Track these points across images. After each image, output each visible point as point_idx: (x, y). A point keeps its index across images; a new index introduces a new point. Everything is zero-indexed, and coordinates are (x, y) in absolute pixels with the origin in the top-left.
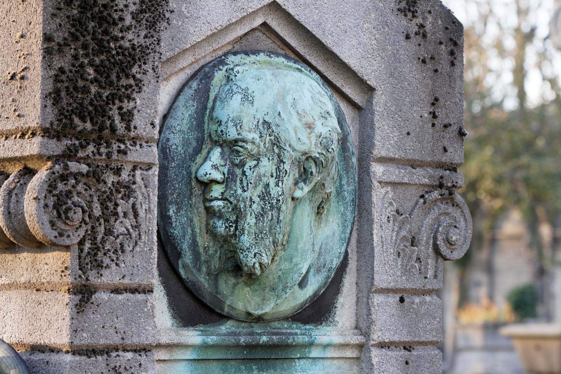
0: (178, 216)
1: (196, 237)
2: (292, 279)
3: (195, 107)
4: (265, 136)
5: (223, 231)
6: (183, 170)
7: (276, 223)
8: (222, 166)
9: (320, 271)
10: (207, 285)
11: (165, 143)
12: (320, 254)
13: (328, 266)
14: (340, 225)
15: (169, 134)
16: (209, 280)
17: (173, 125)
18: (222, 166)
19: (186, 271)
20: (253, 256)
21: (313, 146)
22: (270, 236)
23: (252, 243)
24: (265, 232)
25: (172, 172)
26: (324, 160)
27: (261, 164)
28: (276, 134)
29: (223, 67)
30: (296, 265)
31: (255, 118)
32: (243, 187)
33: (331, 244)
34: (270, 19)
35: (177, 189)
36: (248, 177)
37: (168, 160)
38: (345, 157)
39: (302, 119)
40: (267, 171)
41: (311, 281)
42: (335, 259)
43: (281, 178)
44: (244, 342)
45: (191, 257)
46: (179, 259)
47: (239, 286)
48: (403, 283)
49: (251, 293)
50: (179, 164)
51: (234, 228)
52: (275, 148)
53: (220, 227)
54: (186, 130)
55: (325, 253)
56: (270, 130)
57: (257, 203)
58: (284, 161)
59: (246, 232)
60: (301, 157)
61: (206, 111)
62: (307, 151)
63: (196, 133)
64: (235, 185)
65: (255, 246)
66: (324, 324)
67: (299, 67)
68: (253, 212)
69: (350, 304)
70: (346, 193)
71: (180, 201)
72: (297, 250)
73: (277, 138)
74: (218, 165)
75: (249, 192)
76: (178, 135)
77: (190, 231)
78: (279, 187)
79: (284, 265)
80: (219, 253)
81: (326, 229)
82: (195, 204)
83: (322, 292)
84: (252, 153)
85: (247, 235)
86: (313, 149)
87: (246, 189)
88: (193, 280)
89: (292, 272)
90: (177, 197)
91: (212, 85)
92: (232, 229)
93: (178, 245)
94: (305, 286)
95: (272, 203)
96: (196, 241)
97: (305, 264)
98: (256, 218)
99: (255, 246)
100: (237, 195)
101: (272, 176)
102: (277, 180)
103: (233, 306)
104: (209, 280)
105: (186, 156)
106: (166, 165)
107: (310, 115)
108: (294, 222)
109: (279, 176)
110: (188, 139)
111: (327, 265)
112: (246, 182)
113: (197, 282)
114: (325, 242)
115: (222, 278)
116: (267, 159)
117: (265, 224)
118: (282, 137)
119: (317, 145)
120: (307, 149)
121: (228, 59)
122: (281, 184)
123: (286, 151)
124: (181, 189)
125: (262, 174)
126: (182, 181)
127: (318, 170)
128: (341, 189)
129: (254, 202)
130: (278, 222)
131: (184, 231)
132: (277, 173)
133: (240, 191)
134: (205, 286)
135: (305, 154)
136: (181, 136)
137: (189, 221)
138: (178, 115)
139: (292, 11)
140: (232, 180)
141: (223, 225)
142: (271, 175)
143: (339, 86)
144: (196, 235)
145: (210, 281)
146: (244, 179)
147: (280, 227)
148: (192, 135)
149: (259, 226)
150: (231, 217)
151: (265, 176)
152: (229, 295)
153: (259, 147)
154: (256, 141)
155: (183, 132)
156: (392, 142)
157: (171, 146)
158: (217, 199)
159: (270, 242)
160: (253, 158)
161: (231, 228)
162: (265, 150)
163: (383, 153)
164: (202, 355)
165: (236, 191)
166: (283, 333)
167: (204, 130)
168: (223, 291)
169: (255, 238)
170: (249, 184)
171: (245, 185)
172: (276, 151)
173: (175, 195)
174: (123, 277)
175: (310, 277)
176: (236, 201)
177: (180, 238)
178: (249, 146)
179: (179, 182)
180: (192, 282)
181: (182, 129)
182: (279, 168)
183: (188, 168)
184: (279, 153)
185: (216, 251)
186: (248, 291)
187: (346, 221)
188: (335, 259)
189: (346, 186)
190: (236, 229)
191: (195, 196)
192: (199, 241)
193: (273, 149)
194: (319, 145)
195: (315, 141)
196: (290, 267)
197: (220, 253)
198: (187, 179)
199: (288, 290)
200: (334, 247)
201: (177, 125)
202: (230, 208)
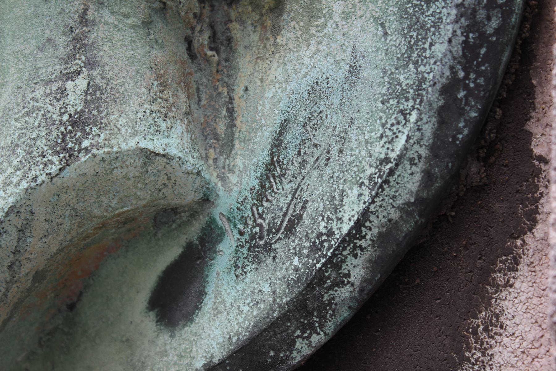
9: (268, 248)
14: (393, 25)
41: (218, 294)
42: (356, 191)
81: (306, 52)
94: (189, 318)
114: (306, 114)
175: (212, 278)
188: (356, 191)
200: (353, 134)
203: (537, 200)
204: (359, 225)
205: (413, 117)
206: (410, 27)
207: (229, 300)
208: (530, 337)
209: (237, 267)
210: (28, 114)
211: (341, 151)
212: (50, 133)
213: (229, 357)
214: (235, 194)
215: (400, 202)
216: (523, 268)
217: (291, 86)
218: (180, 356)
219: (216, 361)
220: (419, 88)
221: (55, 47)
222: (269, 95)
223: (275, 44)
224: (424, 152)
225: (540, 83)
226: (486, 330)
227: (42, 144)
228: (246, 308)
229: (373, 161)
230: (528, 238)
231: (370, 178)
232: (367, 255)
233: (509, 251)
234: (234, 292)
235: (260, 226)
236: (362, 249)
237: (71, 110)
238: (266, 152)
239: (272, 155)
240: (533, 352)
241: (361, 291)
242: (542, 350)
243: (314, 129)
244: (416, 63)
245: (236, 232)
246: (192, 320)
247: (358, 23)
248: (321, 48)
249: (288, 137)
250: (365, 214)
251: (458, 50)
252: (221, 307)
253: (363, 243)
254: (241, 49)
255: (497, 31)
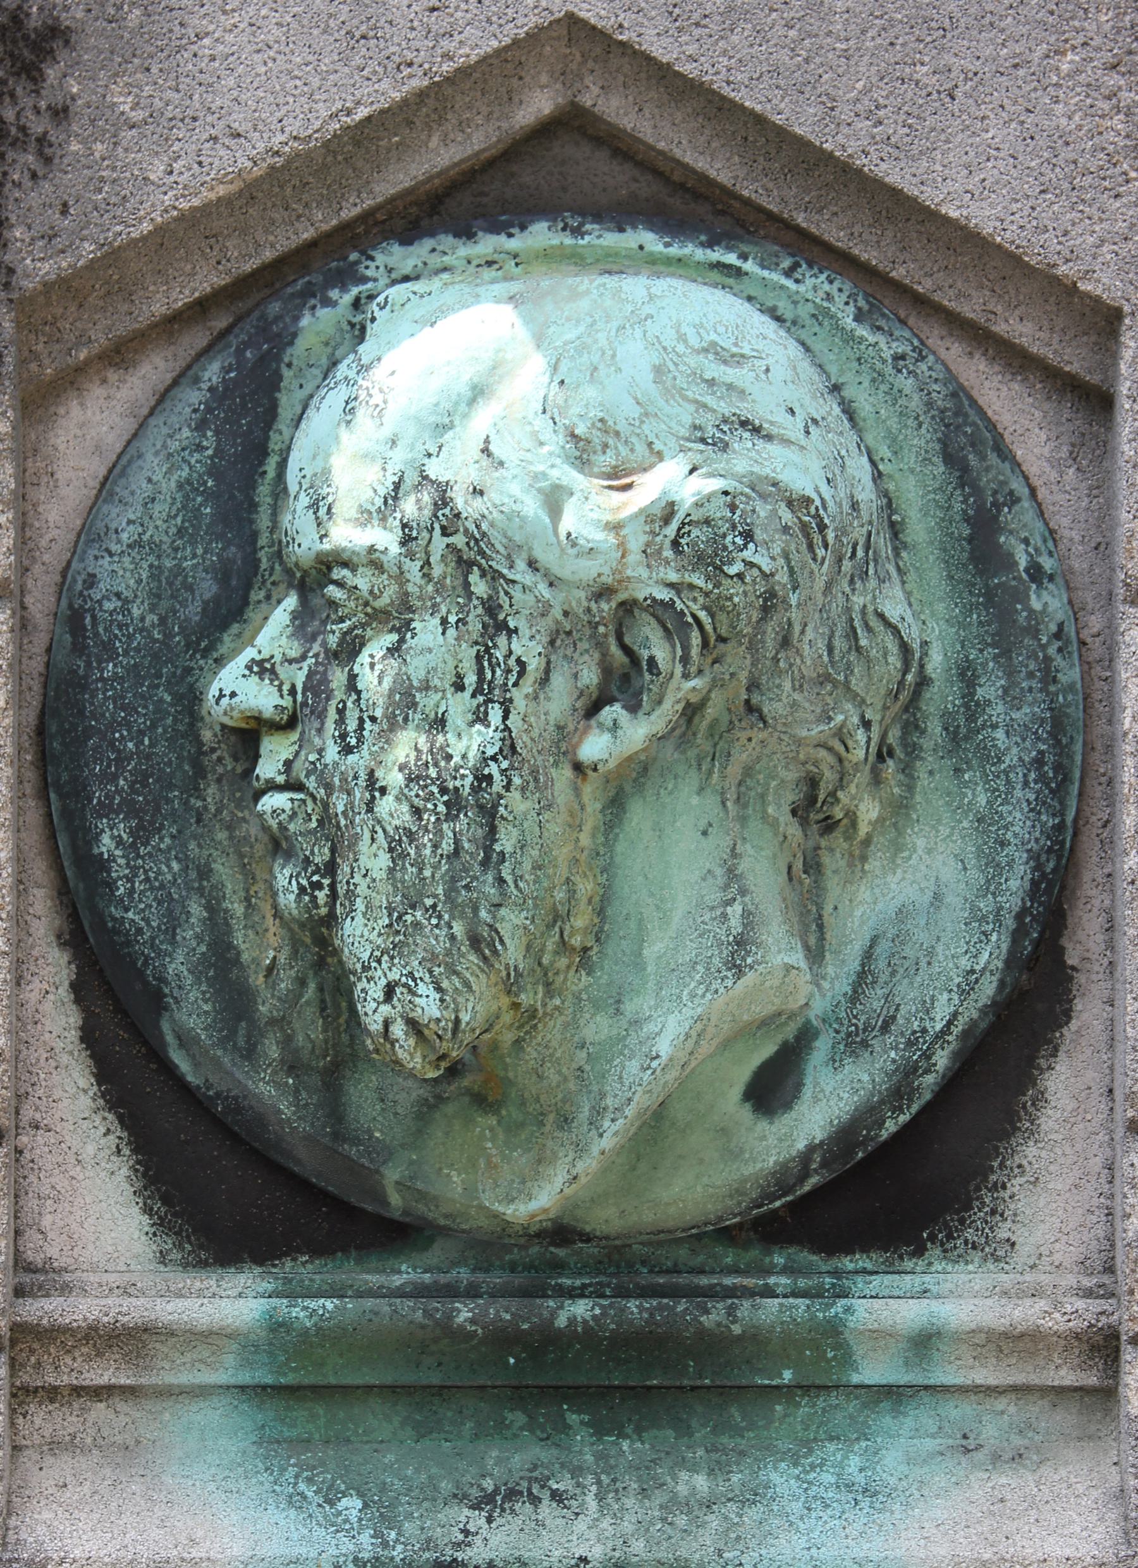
0: (138, 856)
1: (229, 930)
2: (621, 1078)
3: (210, 452)
4: (425, 534)
5: (293, 905)
6: (157, 686)
7: (477, 867)
8: (291, 662)
9: (865, 1044)
10: (286, 1109)
11: (81, 594)
12: (863, 978)
13: (908, 1020)
14: (972, 862)
15: (96, 558)
16: (297, 1092)
17: (113, 526)
18: (291, 662)
19: (193, 1057)
20: (380, 995)
21: (634, 557)
22: (453, 917)
23: (378, 947)
24: (429, 902)
25: (106, 698)
26: (704, 608)
27: (410, 642)
28: (472, 527)
29: (344, 289)
30: (636, 1023)
31: (384, 469)
32: (343, 736)
33: (922, 937)
34: (595, 90)
35: (129, 759)
36: (364, 695)
37: (89, 656)
38: (989, 595)
39: (593, 458)
40: (435, 669)
41: (816, 1084)
42: (945, 996)
43: (497, 692)
44: (472, 1321)
45: (206, 1008)
46: (159, 1015)
47: (450, 1109)
49: (501, 1136)
50: (136, 665)
51: (326, 891)
52: (474, 577)
53: (286, 890)
54: (165, 539)
55: (893, 973)
56: (447, 511)
57: (394, 792)
58: (512, 625)
59: (360, 905)
60: (593, 605)
61: (261, 463)
62: (608, 580)
63: (217, 546)
64: (320, 731)
65: (392, 958)
66: (933, 1252)
67: (731, 258)
68: (378, 828)
69: (1078, 1174)
70: (1000, 734)
71: (147, 802)
72: (639, 965)
73: (476, 541)
74: (278, 659)
75: (365, 753)
76: (126, 560)
77: (196, 909)
78: (488, 726)
79: (592, 1025)
80: (312, 986)
81: (893, 880)
82: (219, 811)
83: (891, 1127)
84: (379, 603)
85: (364, 914)
86: (636, 568)
87: (353, 742)
88: (229, 1090)
89: (622, 1053)
90: (131, 787)
91: (289, 365)
92: (322, 896)
93: (146, 963)
94: (788, 1106)
95: (456, 789)
96: (230, 946)
97: (672, 1020)
98: (391, 850)
99: (392, 958)
100: (326, 765)
101: (459, 687)
102: (481, 699)
103: (419, 1185)
104: (297, 1092)
105: (168, 635)
106: (81, 672)
107: (634, 439)
108: (618, 859)
109: (490, 682)
110: (178, 570)
111: (901, 1021)
112: (357, 714)
113: (245, 1097)
114: (895, 931)
115: (359, 1081)
116: (436, 621)
117: (427, 873)
118: (493, 533)
119: (659, 552)
120: (606, 570)
121: (372, 259)
122: (500, 713)
123: (518, 587)
124: (148, 757)
125: (415, 683)
126: (154, 726)
127: (679, 653)
128: (971, 718)
129: (383, 791)
130: (485, 863)
131: (170, 912)
132: (480, 672)
133: (332, 753)
134: (280, 1112)
135: (603, 592)
136: (145, 565)
137: (193, 875)
138: (134, 487)
139: (660, 49)
140: (312, 712)
141: (294, 882)
142: (454, 685)
143: (972, 315)
144: (227, 924)
145: (304, 1095)
146: (349, 704)
147: (501, 881)
148: (194, 556)
149: (403, 882)
150: (316, 850)
151: (427, 688)
152: (402, 1146)
153: (400, 577)
154: (383, 558)
155: (155, 547)
157: (99, 602)
158: (272, 786)
159: (453, 938)
160: (387, 622)
161: (317, 893)
162: (430, 588)
164: (295, 1370)
165: (320, 751)
166: (698, 1287)
167: (255, 535)
168: (369, 1132)
169: (390, 925)
170: (368, 725)
171: (352, 725)
172: (480, 587)
173: (122, 782)
175: (809, 1069)
176: (322, 791)
177: (153, 938)
178: (362, 581)
179: (141, 733)
180: (227, 1098)
181: (145, 538)
182: (490, 655)
183: (182, 678)
184: (490, 598)
185: (302, 982)
186: (492, 1130)
187: (1003, 844)
188: (945, 996)
189: (1000, 708)
190: (333, 895)
191: (219, 781)
192: (243, 947)
193: (467, 585)
194: (668, 553)
195: (644, 538)
196: (615, 1032)
197: (321, 989)
198: (175, 720)
199: (607, 1124)
200: (940, 949)
201: (124, 524)
202: (314, 818)
203: (1071, 1001)
204: (950, 1023)
205: (994, 937)
206: (987, 865)
207: (828, 1089)
208: (1069, 1108)
209: (834, 1061)
210: (700, 936)
211: (929, 963)
212: (721, 952)
213: (830, 1138)
214: (828, 998)
215: (980, 1004)
216: (1061, 1055)
217: (880, 906)
218: (780, 1140)
219: (817, 1141)
220: (998, 914)
221: (714, 877)
222: (858, 913)
223: (863, 870)
224: (1000, 965)
225: (1070, 908)
226: (1033, 1104)
227: (716, 961)
228: (846, 1095)
229: (960, 971)
230: (1065, 1030)
231: (959, 986)
232: (952, 1047)
233: (1049, 1042)
234: (832, 1082)
235: (856, 1025)
236: (949, 1043)
237: (734, 932)
238: (857, 962)
239: (863, 965)
240: (1072, 1120)
241: (944, 1076)
242: (1080, 1118)
243: (902, 943)
244: (994, 894)
245: (831, 1031)
246: (791, 1108)
247: (940, 858)
248: (907, 876)
249: (878, 950)
250: (955, 1015)
251: (1027, 885)
252: (821, 1096)
253: (950, 1038)
254: (829, 873)
255: (1054, 871)
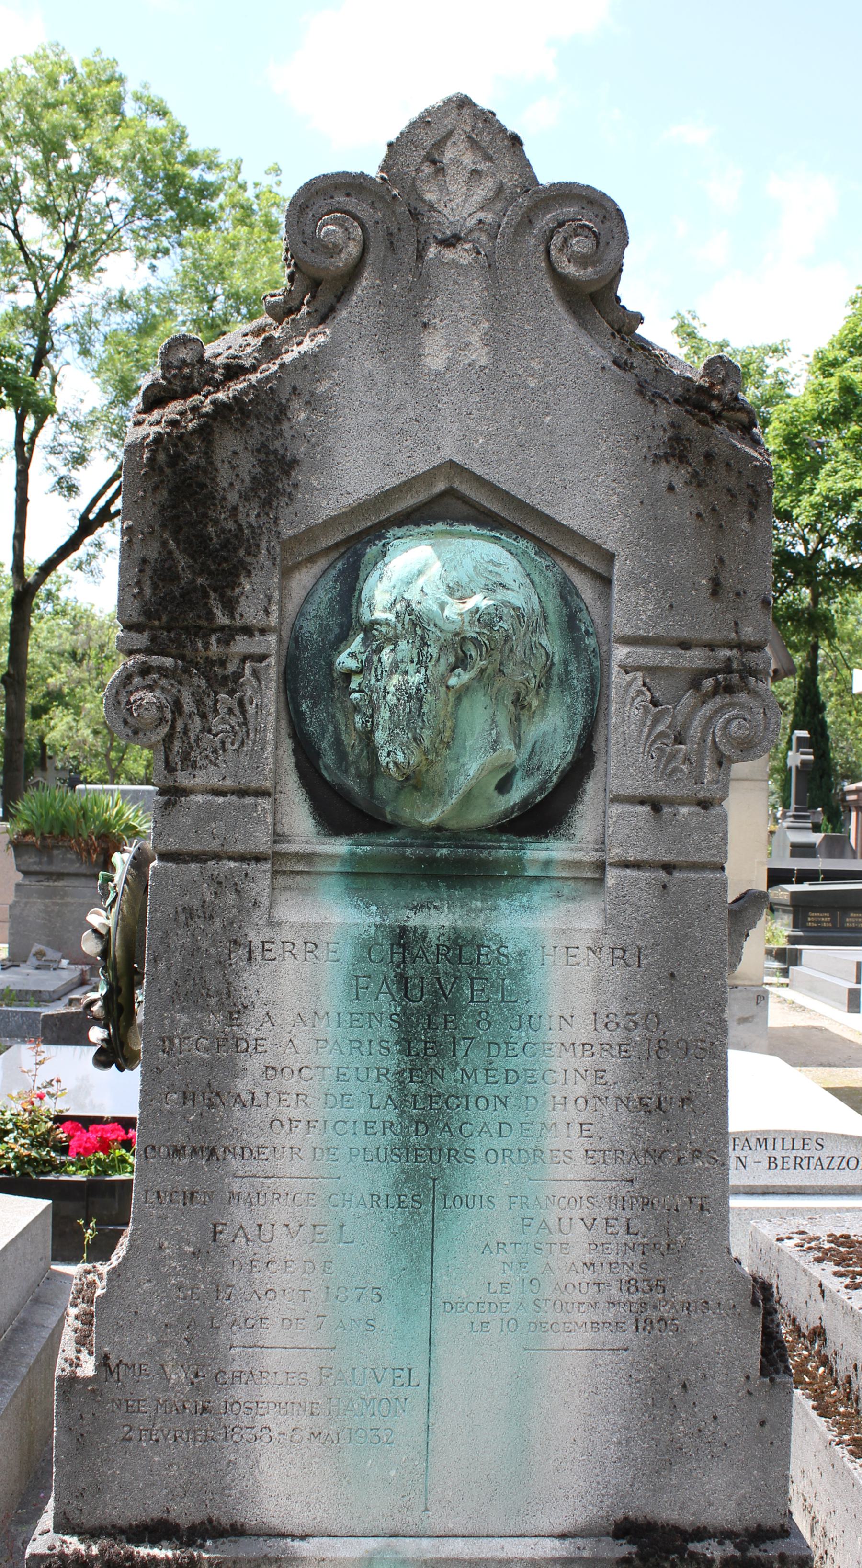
1: (340, 734)
10: (357, 789)
12: (532, 754)
13: (545, 766)
21: (466, 624)
30: (463, 765)
33: (550, 741)
47: (406, 790)
48: (659, 788)
67: (498, 535)
72: (465, 748)
77: (331, 728)
83: (539, 799)
86: (466, 627)
101: (412, 662)
105: (324, 644)
110: (328, 625)
130: (419, 716)
133: (373, 681)
135: (456, 634)
139: (478, 471)
153: (395, 628)
156: (643, 617)
158: (355, 691)
163: (628, 631)
172: (419, 632)
174: (224, 778)
178: (384, 629)
